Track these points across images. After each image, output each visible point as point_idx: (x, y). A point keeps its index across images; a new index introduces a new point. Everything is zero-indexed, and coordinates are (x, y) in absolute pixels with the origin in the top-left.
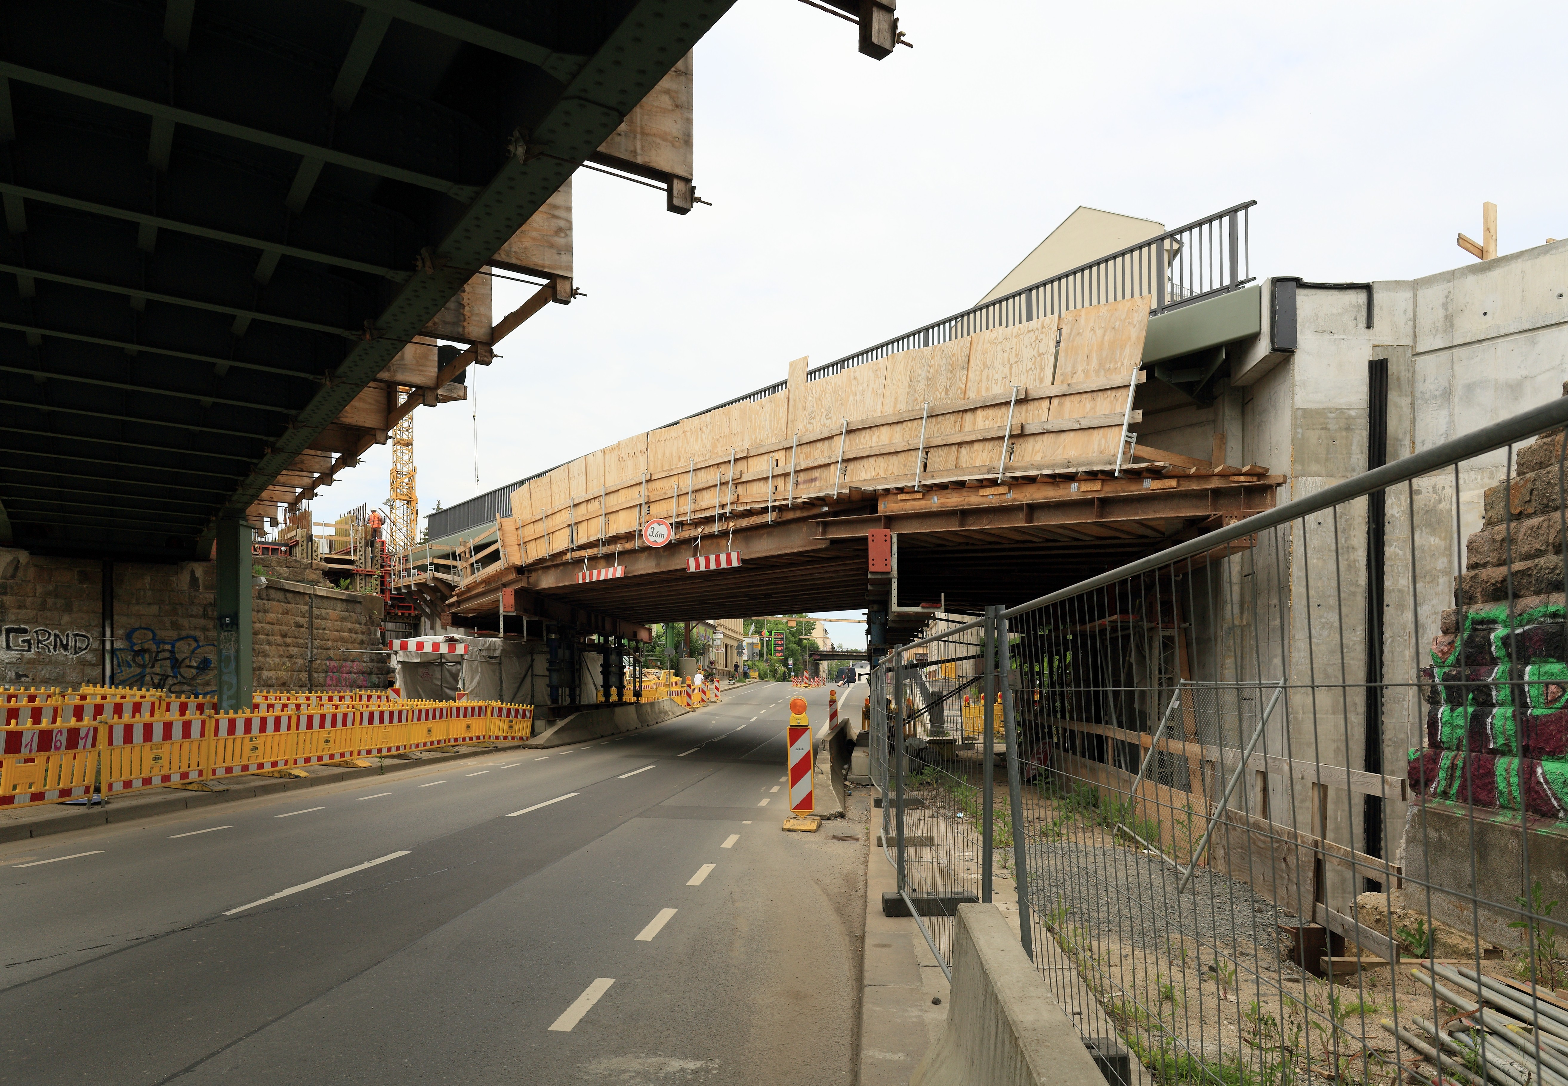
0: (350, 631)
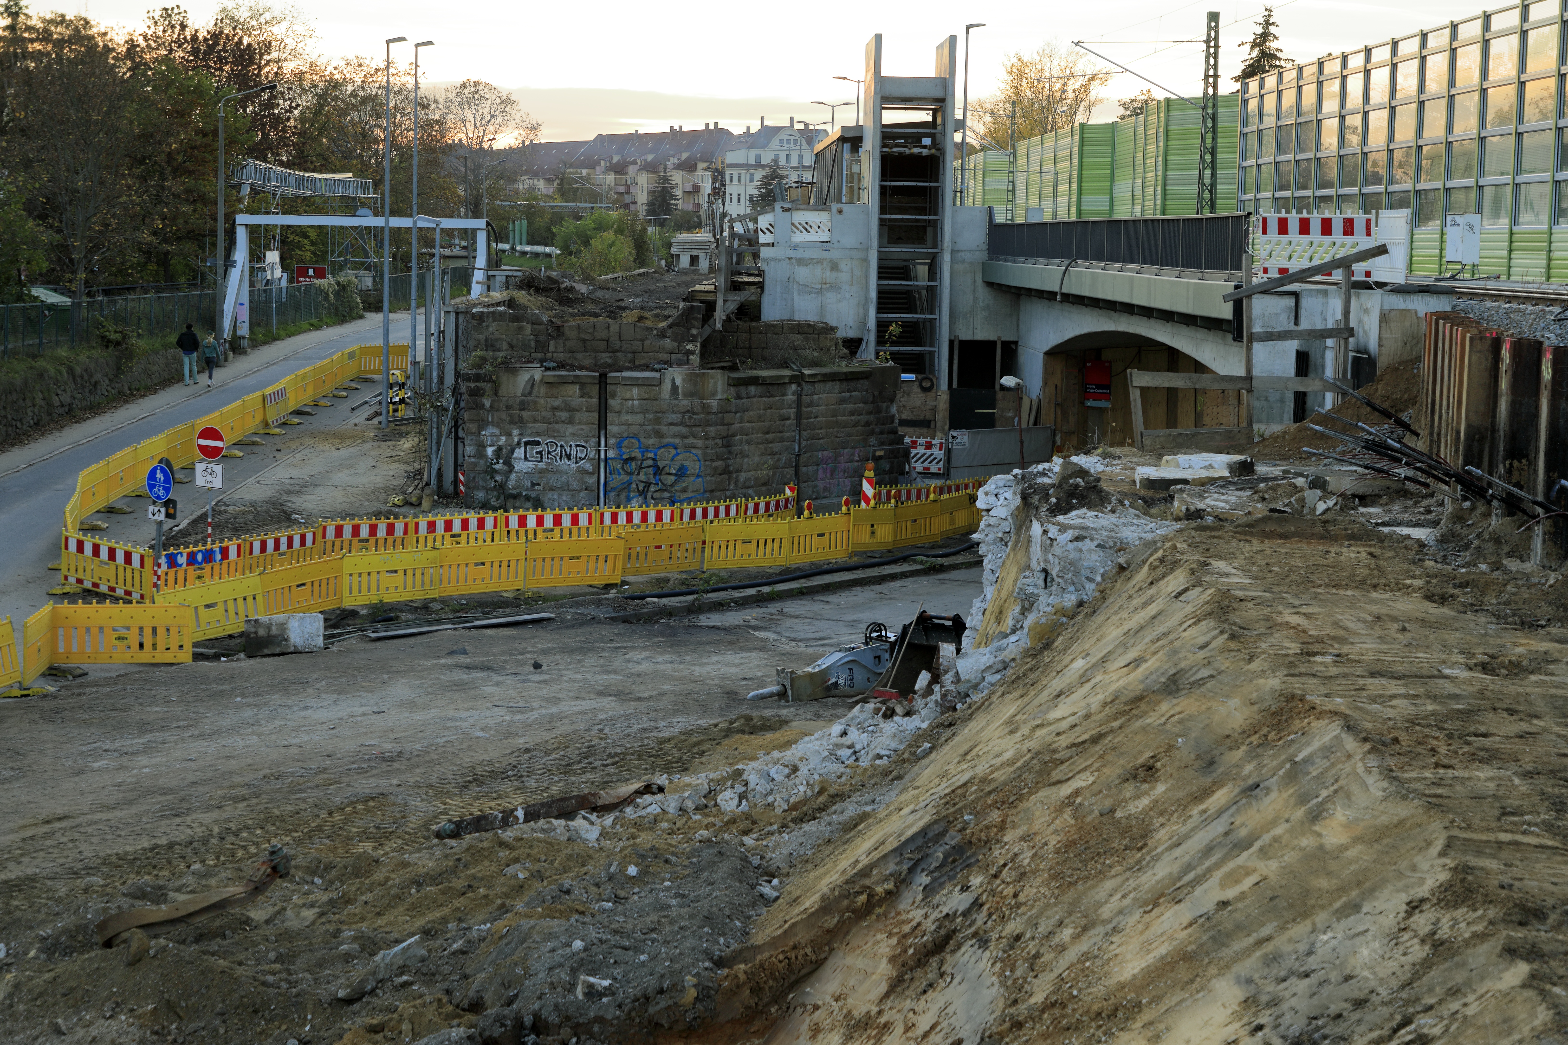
0: (852, 413)
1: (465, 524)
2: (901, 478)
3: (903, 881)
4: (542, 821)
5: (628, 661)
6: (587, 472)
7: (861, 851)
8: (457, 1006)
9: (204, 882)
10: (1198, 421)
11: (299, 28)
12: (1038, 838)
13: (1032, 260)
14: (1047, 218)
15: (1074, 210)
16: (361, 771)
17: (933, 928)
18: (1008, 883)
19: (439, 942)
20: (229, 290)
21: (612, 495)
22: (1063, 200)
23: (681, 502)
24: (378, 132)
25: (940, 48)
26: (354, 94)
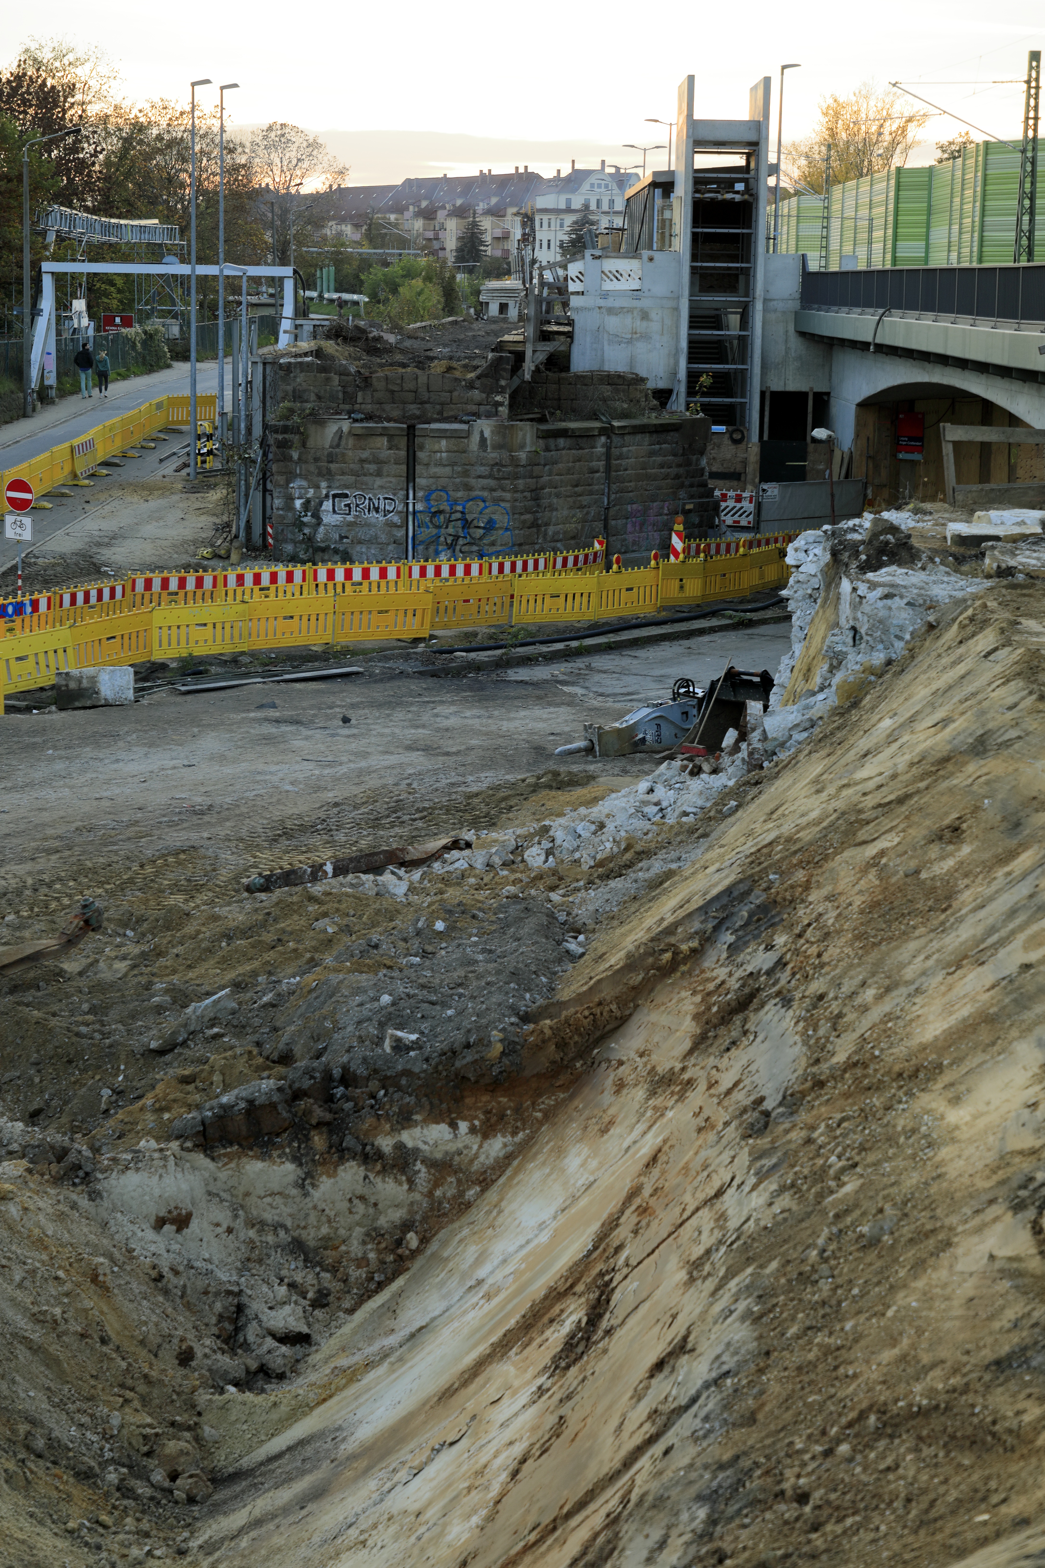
0: (662, 466)
1: (274, 578)
2: (710, 531)
3: (707, 939)
4: (351, 876)
5: (437, 715)
6: (396, 526)
7: (666, 909)
8: (267, 1058)
9: (18, 934)
10: (1012, 476)
11: (103, 70)
12: (843, 898)
13: (846, 309)
14: (862, 266)
15: (889, 256)
16: (172, 824)
17: (737, 986)
18: (812, 943)
19: (249, 995)
20: (36, 339)
21: (420, 548)
22: (877, 247)
23: (489, 556)
24: (184, 176)
25: (754, 89)
26: (159, 138)
